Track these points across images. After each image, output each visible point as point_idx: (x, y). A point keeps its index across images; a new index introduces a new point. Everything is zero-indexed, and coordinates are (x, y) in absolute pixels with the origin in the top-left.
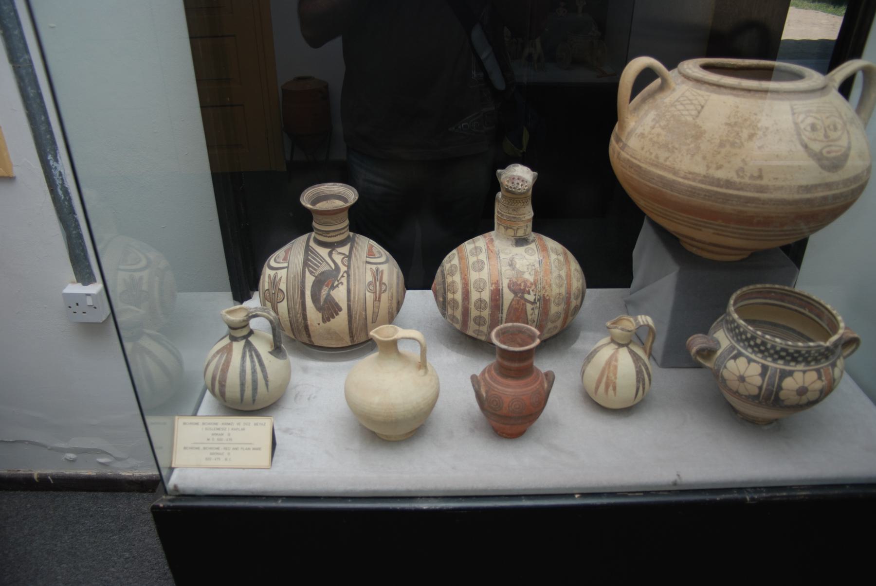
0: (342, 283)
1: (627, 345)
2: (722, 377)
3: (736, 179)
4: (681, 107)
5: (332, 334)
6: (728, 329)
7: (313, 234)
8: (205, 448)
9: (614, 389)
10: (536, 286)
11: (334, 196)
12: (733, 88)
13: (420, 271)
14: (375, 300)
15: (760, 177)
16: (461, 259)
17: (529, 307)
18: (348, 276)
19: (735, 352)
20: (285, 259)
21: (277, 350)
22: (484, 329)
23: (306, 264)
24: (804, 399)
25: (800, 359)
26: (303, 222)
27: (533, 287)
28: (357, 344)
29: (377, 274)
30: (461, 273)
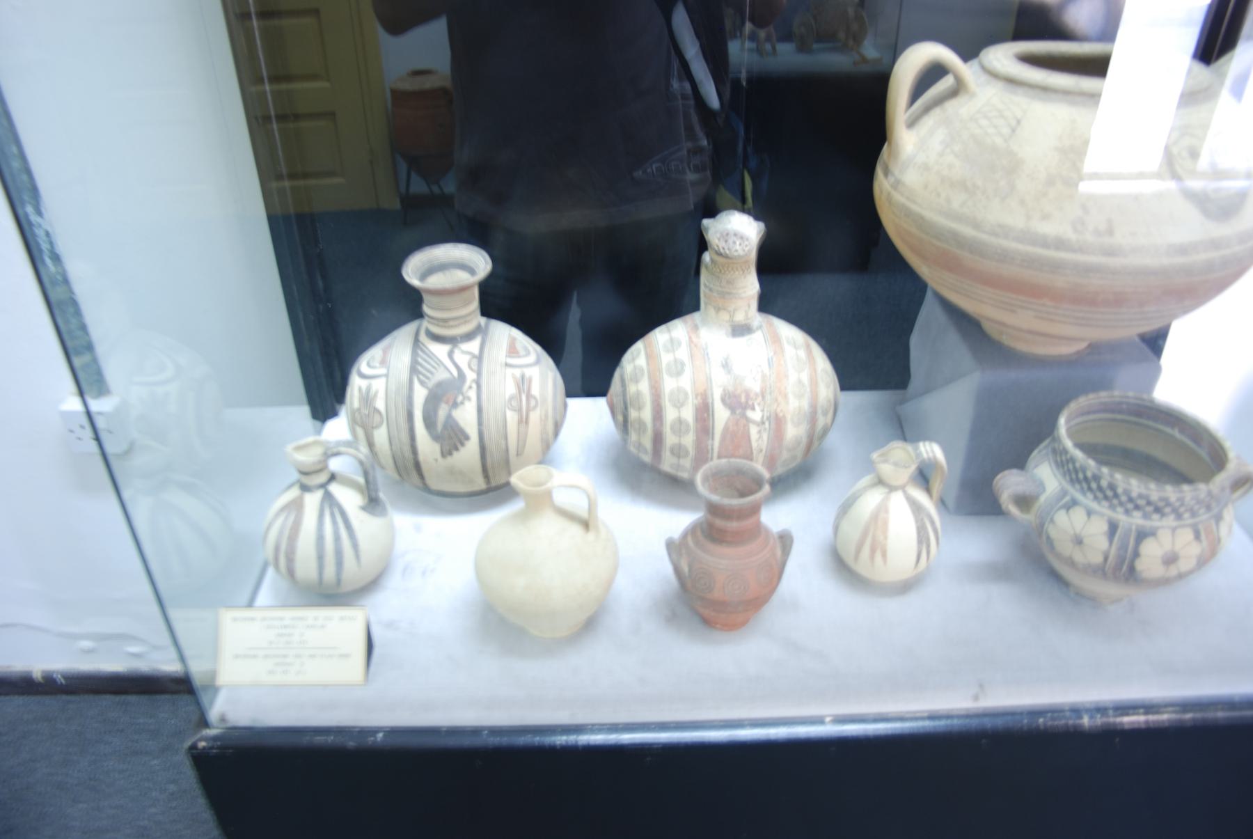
0: (469, 399)
1: (903, 488)
2: (1048, 537)
3: (1070, 235)
4: (984, 122)
5: (453, 472)
6: (1056, 462)
7: (425, 324)
8: (266, 656)
9: (884, 555)
10: (763, 397)
11: (451, 268)
12: (1065, 93)
13: (592, 372)
14: (520, 421)
15: (1110, 232)
16: (649, 357)
17: (754, 431)
18: (479, 387)
19: (1067, 499)
20: (383, 362)
21: (373, 503)
22: (687, 463)
23: (414, 370)
24: (1173, 571)
25: (1167, 510)
26: (410, 304)
27: (760, 399)
28: (492, 488)
29: (523, 384)
30: (650, 378)
